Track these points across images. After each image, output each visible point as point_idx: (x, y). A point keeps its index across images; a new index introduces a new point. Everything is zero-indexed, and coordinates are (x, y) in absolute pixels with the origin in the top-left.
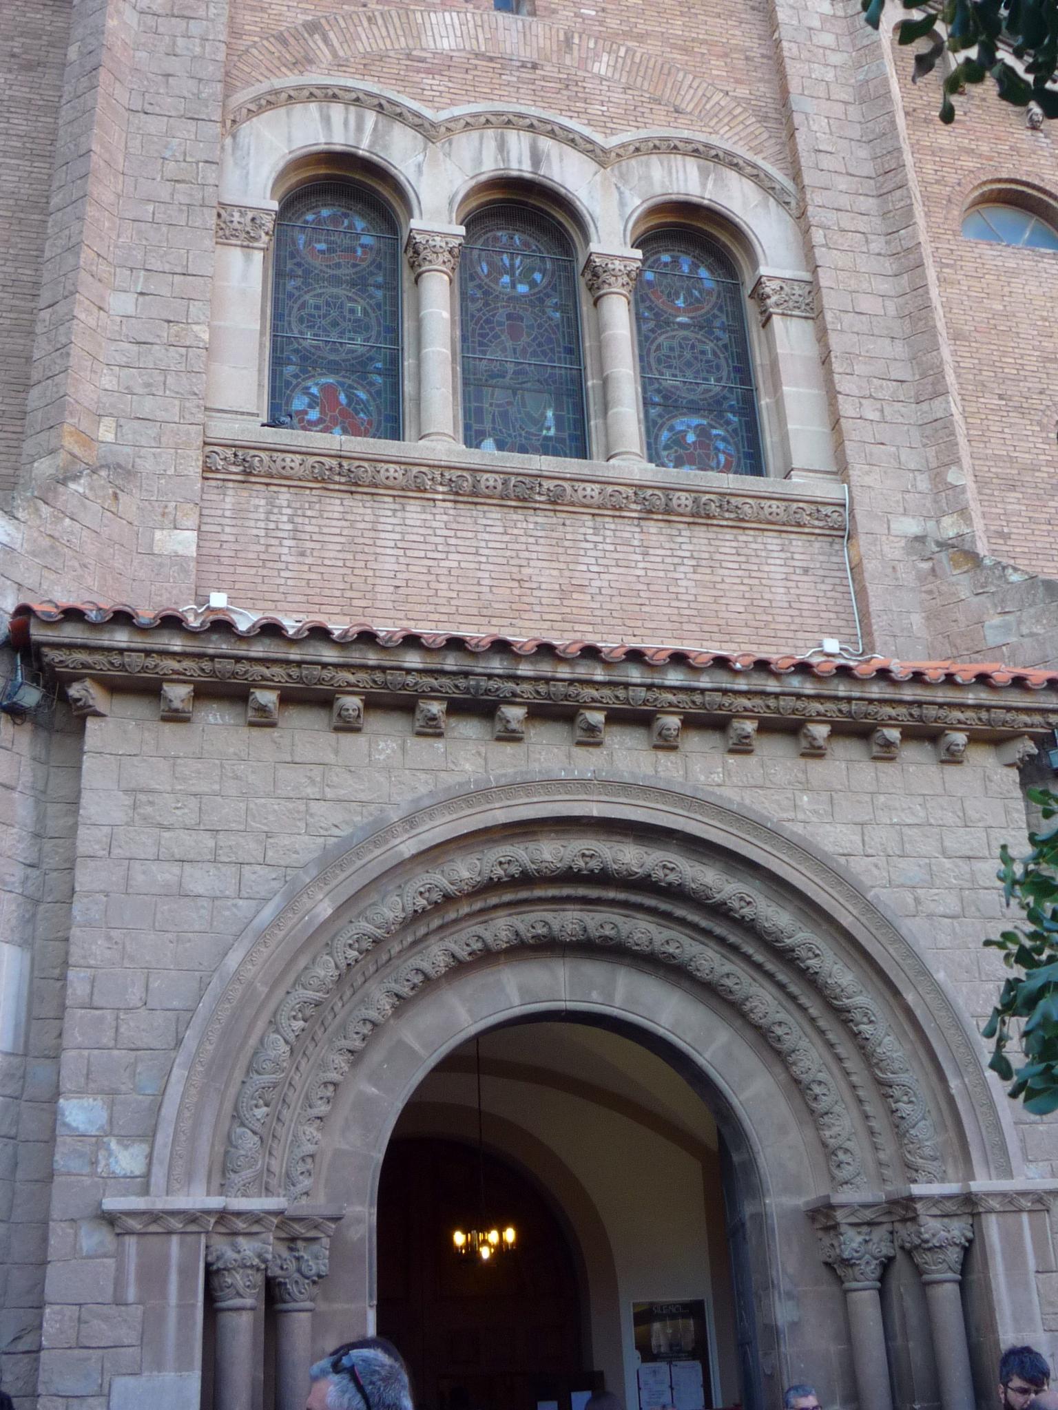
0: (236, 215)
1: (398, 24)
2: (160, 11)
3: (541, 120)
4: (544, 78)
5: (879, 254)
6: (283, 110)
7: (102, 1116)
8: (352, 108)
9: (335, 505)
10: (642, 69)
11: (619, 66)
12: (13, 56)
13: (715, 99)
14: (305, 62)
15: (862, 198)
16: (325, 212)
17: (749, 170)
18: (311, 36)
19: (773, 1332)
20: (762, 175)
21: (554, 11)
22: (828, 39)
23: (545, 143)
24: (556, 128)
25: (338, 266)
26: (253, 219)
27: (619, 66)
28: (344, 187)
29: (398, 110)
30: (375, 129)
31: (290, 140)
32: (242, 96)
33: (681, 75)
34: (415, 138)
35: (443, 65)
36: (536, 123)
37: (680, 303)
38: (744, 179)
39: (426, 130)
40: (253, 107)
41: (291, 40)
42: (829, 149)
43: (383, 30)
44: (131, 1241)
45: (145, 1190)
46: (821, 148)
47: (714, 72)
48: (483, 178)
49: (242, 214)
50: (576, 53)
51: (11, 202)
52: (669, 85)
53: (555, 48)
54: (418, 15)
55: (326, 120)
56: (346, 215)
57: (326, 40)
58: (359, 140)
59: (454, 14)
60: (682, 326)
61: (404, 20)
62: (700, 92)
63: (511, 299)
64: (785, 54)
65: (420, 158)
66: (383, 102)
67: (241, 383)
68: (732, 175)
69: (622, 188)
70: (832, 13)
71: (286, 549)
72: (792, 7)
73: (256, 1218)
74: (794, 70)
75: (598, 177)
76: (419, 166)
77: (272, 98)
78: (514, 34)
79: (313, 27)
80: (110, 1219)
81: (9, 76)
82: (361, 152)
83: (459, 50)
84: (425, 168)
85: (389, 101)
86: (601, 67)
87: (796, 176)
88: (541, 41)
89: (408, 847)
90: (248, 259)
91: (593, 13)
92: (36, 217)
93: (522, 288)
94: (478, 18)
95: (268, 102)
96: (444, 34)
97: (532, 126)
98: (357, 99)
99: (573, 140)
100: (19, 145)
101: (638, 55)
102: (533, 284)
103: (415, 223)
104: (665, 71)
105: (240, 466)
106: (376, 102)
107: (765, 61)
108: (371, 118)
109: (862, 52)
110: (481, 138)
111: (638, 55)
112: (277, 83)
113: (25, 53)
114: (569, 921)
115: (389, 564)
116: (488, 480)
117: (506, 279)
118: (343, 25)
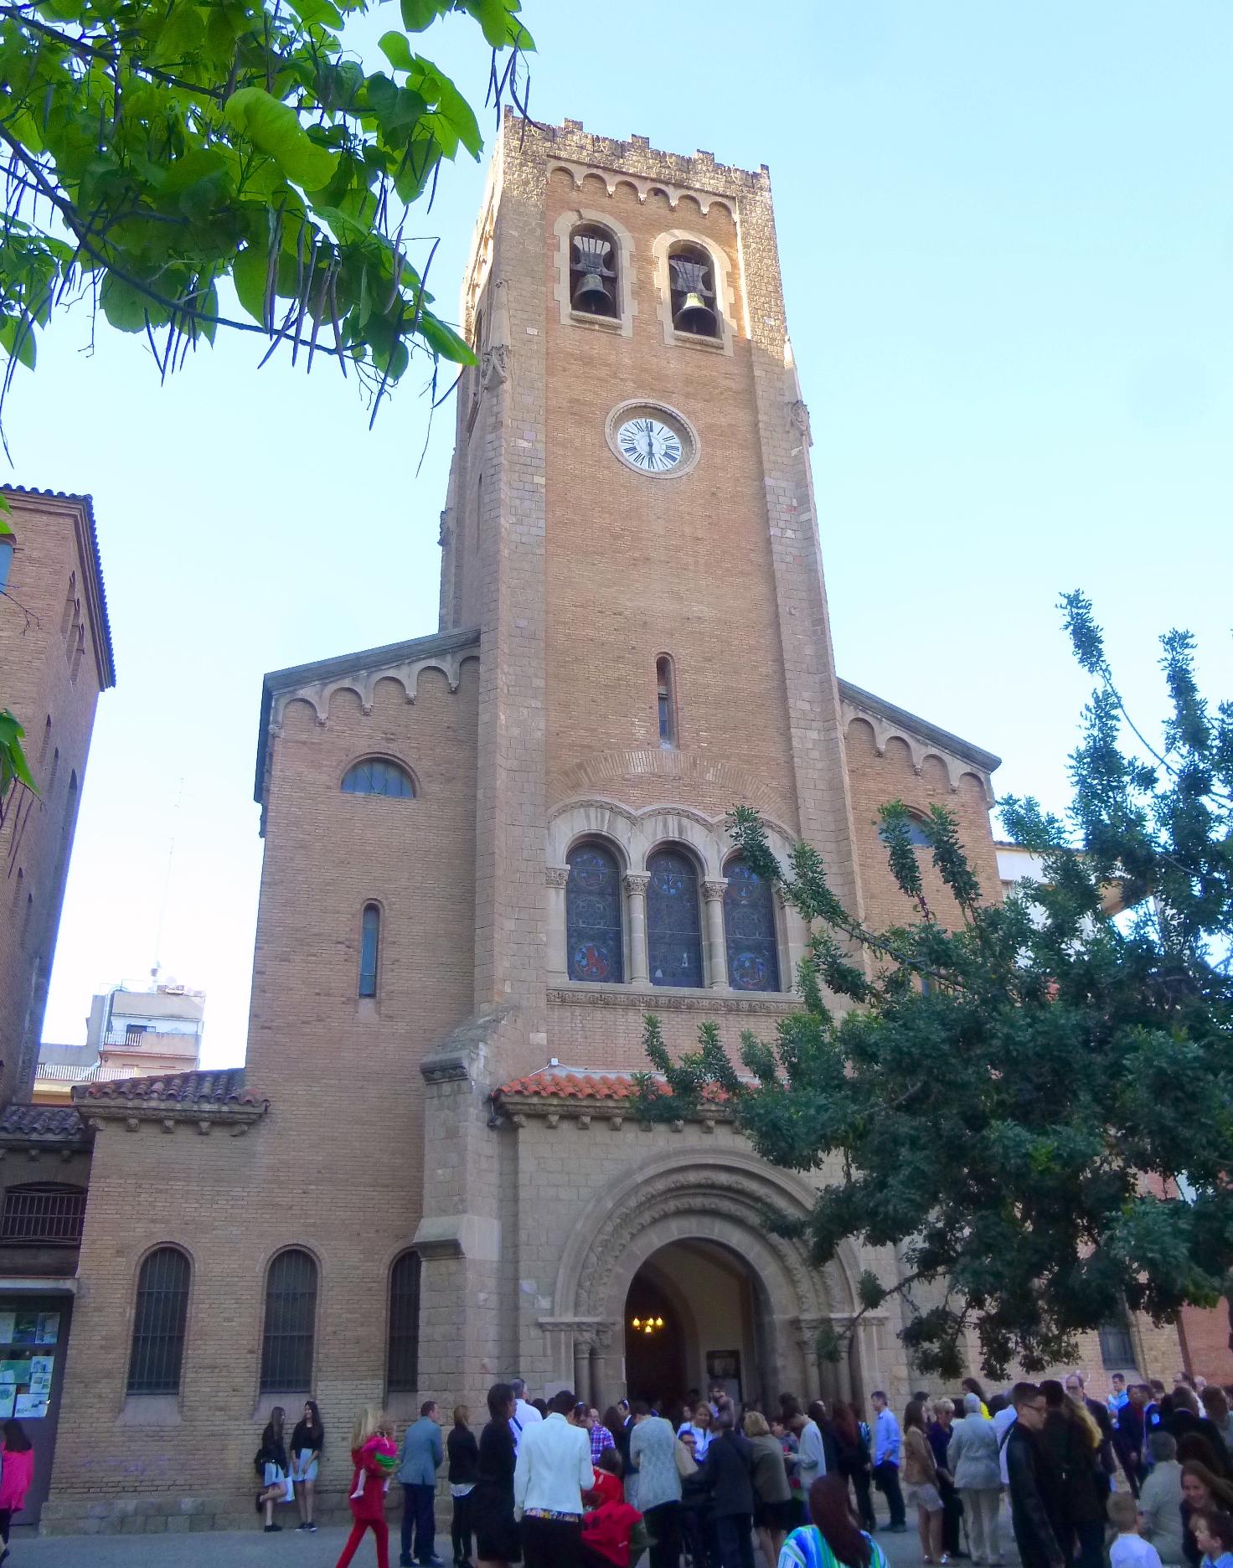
7: (535, 1286)
9: (598, 1015)
14: (576, 786)
19: (775, 1371)
22: (815, 754)
23: (685, 821)
28: (597, 850)
35: (637, 782)
39: (633, 821)
44: (548, 1334)
45: (552, 1314)
55: (588, 816)
67: (557, 958)
73: (589, 1325)
79: (580, 766)
80: (541, 1326)
86: (709, 777)
87: (799, 832)
89: (640, 1178)
103: (629, 872)
105: (561, 999)
108: (607, 814)
112: (567, 801)
114: (698, 1202)
115: (621, 1041)
116: (662, 1001)
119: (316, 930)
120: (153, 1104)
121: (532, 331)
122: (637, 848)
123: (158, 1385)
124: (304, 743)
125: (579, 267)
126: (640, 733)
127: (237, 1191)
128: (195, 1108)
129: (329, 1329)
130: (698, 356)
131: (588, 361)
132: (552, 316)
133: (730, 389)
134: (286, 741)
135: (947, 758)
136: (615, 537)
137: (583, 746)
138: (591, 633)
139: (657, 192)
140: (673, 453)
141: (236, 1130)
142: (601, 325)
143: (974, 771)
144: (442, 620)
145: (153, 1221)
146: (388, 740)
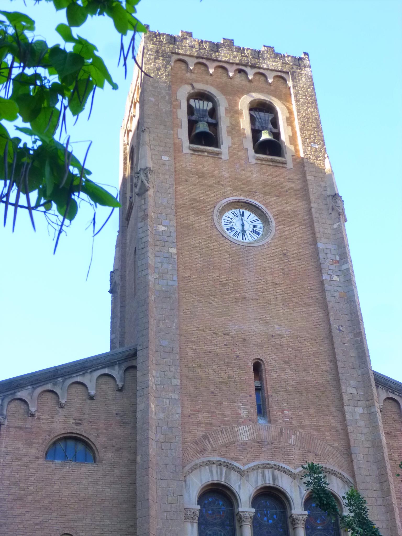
0: (189, 512)
1: (230, 433)
2: (162, 441)
3: (275, 465)
4: (275, 448)
5: (380, 505)
6: (198, 470)
8: (219, 467)
10: (304, 440)
11: (297, 440)
12: (113, 446)
13: (328, 448)
14: (203, 451)
15: (374, 484)
16: (210, 499)
17: (339, 475)
18: (205, 440)
20: (343, 477)
21: (277, 421)
22: (362, 423)
23: (277, 472)
24: (280, 468)
25: (215, 519)
26: (193, 513)
27: (297, 440)
28: (218, 494)
29: (232, 467)
30: (226, 473)
31: (201, 481)
32: (188, 468)
33: (316, 440)
34: (238, 475)
36: (273, 466)
37: (319, 521)
38: (338, 479)
39: (241, 473)
40: (190, 471)
41: (199, 443)
42: (364, 467)
43: (226, 435)
46: (361, 467)
47: (327, 438)
48: (258, 488)
49: (190, 511)
50: (284, 436)
51: (117, 501)
52: (313, 445)
53: (277, 435)
54: (236, 428)
55: (211, 472)
56: (216, 500)
57: (209, 441)
58: (221, 478)
59: (246, 426)
60: (320, 530)
61: (232, 431)
62: (323, 447)
64: (349, 431)
65: (240, 483)
66: (228, 464)
68: (334, 477)
69: (301, 487)
70: (363, 412)
72: (350, 412)
74: (352, 437)
75: (293, 484)
76: (239, 486)
77: (195, 467)
78: (265, 431)
79: (205, 437)
81: (113, 454)
82: (222, 483)
83: (249, 440)
84: (241, 487)
85: (230, 464)
86: (292, 441)
87: (354, 477)
88: (273, 433)
90: (192, 526)
91: (288, 420)
92: (124, 506)
93: (271, 521)
94: (253, 427)
95: (194, 468)
96: (244, 434)
97: (272, 467)
98: (220, 464)
99: (285, 471)
100: (117, 480)
101: (303, 434)
103: (240, 509)
104: (312, 440)
106: (225, 464)
107: (343, 431)
109: (373, 428)
110: (257, 473)
111: (303, 434)
113: (116, 444)
117: (265, 518)
118: (214, 435)
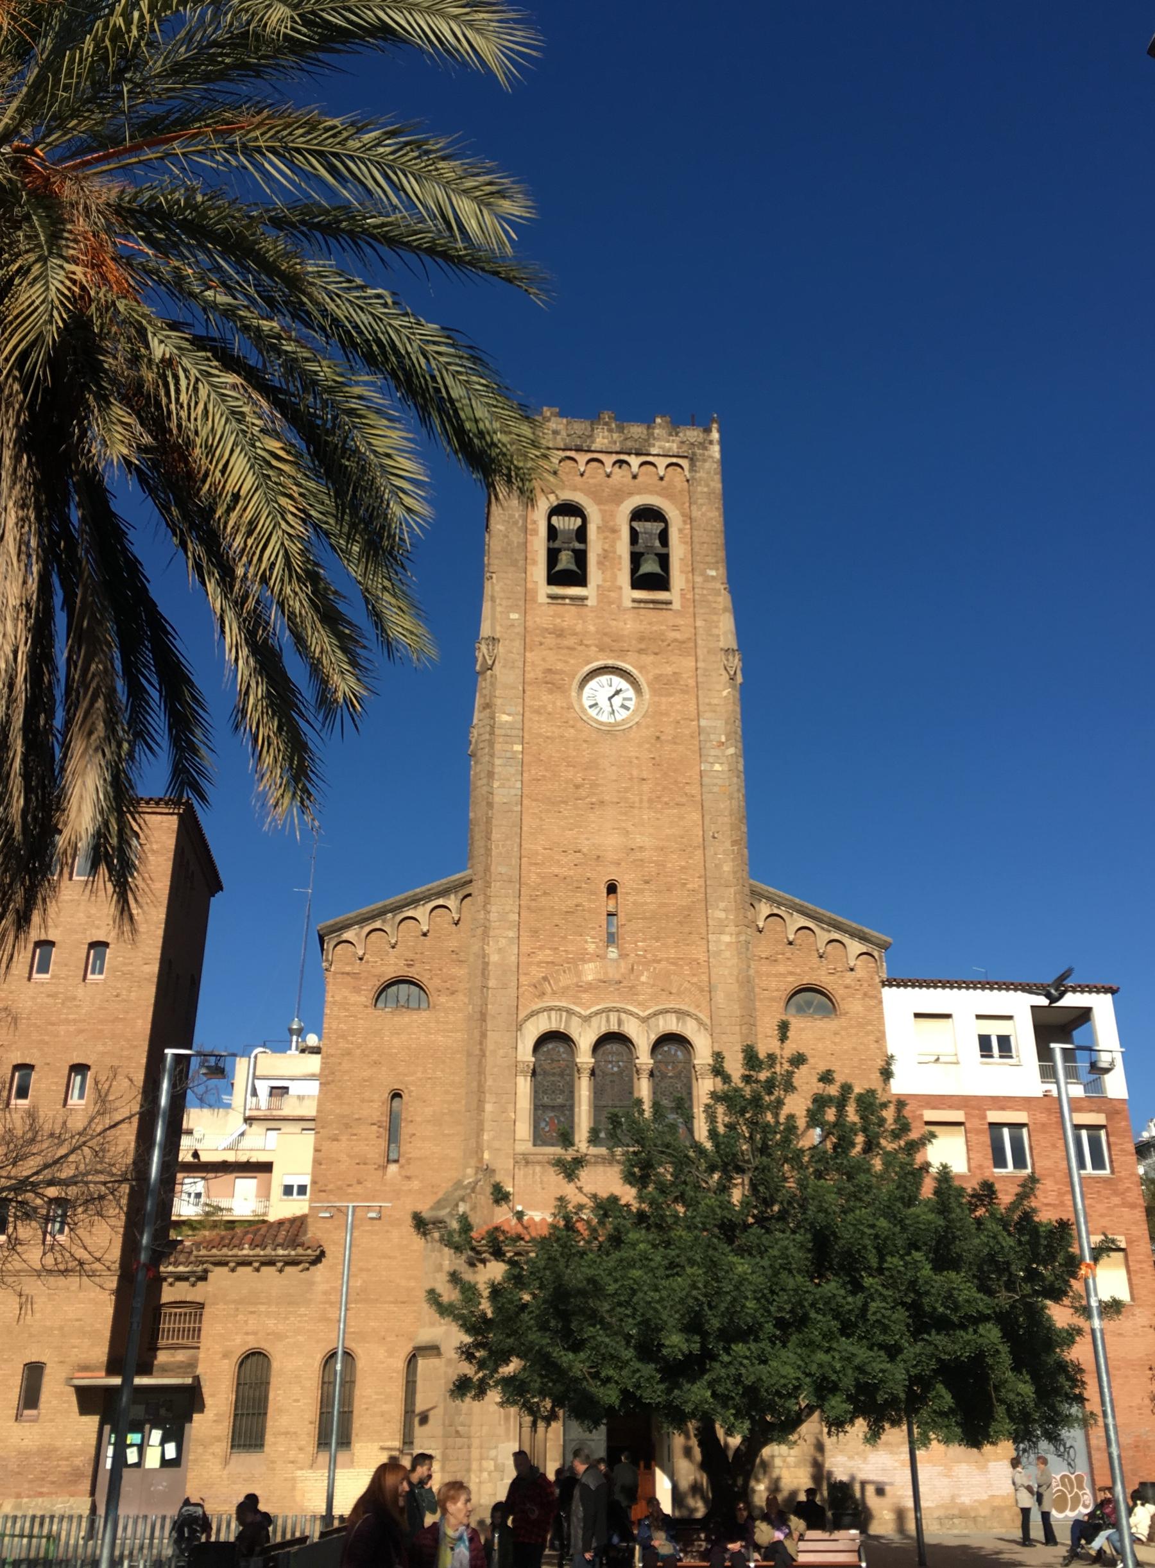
22: (727, 954)
23: (623, 1016)
35: (589, 987)
55: (550, 1018)
60: (671, 1077)
63: (613, 1074)
67: (524, 1129)
68: (688, 1018)
71: (538, 1188)
79: (545, 979)
86: (643, 979)
93: (616, 1069)
102: (619, 1067)
108: (564, 1014)
119: (357, 1116)
120: (245, 1252)
121: (514, 616)
122: (643, 1040)
123: (250, 1446)
124: (348, 974)
125: (557, 545)
126: (591, 948)
127: (302, 1310)
128: (273, 1253)
129: (364, 1406)
130: (652, 613)
131: (560, 633)
132: (528, 596)
133: (676, 640)
134: (335, 973)
135: (846, 939)
136: (577, 787)
137: (547, 963)
138: (556, 871)
139: (621, 463)
140: (627, 703)
141: (301, 1267)
142: (572, 598)
143: (870, 950)
144: (938, 1548)
145: (247, 1334)
146: (409, 966)
